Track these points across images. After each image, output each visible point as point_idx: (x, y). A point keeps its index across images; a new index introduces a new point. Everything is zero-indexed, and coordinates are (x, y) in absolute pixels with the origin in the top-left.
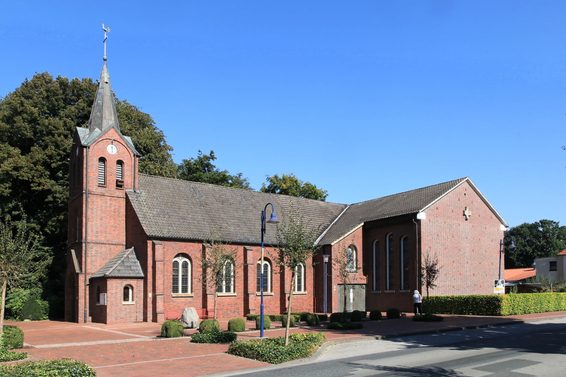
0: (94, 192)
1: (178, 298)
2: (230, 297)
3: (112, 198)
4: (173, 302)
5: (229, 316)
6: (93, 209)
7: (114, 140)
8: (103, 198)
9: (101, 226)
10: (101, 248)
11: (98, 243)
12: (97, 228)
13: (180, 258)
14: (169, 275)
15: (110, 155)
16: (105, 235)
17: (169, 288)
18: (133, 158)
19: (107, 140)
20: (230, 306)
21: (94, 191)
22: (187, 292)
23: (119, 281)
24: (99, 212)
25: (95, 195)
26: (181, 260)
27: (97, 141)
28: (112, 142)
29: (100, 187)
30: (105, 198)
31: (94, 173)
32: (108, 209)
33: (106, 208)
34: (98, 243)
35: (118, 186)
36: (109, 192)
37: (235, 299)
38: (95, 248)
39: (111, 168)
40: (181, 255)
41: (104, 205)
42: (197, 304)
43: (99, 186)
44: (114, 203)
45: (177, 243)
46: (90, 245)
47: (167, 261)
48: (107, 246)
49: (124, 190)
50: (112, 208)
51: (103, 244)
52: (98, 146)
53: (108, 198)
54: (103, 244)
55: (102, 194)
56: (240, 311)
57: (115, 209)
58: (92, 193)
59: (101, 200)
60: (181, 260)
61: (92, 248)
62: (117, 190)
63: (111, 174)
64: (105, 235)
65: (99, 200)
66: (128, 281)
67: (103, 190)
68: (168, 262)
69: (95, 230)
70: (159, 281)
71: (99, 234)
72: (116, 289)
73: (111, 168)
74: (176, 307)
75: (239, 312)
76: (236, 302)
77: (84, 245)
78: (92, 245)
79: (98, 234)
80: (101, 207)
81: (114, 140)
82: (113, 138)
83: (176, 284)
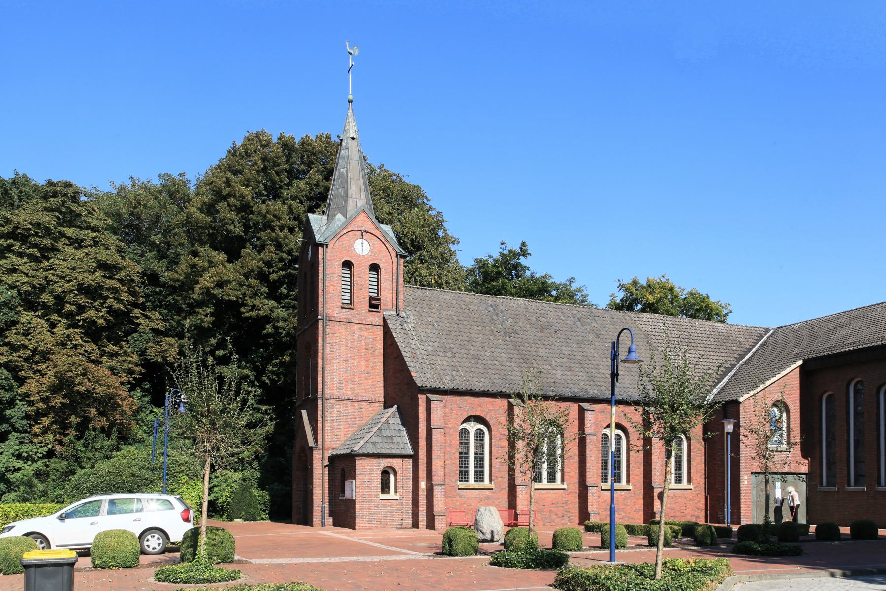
0: (334, 317)
1: (468, 491)
2: (555, 491)
3: (362, 325)
4: (460, 497)
5: (554, 524)
6: (334, 344)
7: (365, 231)
8: (349, 326)
9: (346, 371)
10: (347, 406)
11: (341, 400)
12: (340, 375)
13: (472, 423)
14: (453, 452)
15: (359, 256)
16: (352, 386)
17: (453, 474)
18: (395, 259)
19: (355, 232)
20: (554, 505)
21: (336, 315)
22: (482, 481)
23: (374, 461)
24: (343, 349)
25: (337, 323)
26: (472, 427)
27: (339, 235)
28: (362, 235)
29: (344, 310)
30: (351, 326)
31: (335, 287)
32: (356, 344)
33: (353, 343)
34: (341, 400)
35: (372, 306)
36: (358, 317)
37: (563, 495)
38: (338, 407)
39: (360, 277)
40: (472, 419)
41: (350, 337)
42: (500, 500)
43: (342, 308)
44: (365, 334)
45: (466, 398)
46: (329, 403)
47: (450, 429)
48: (356, 404)
49: (382, 313)
50: (363, 343)
51: (349, 400)
52: (341, 243)
53: (357, 326)
54: (349, 400)
55: (347, 320)
56: (572, 515)
57: (367, 344)
58: (332, 319)
59: (346, 329)
60: (472, 427)
61: (332, 408)
62: (370, 313)
63: (360, 287)
64: (352, 386)
65: (342, 330)
66: (387, 461)
67: (349, 313)
68: (452, 430)
69: (336, 378)
70: (437, 462)
71: (343, 385)
72: (370, 474)
73: (360, 277)
74: (465, 505)
75: (571, 516)
76: (566, 499)
77: (320, 402)
78: (332, 402)
79: (341, 385)
80: (346, 340)
81: (365, 231)
82: (363, 229)
83: (465, 467)
